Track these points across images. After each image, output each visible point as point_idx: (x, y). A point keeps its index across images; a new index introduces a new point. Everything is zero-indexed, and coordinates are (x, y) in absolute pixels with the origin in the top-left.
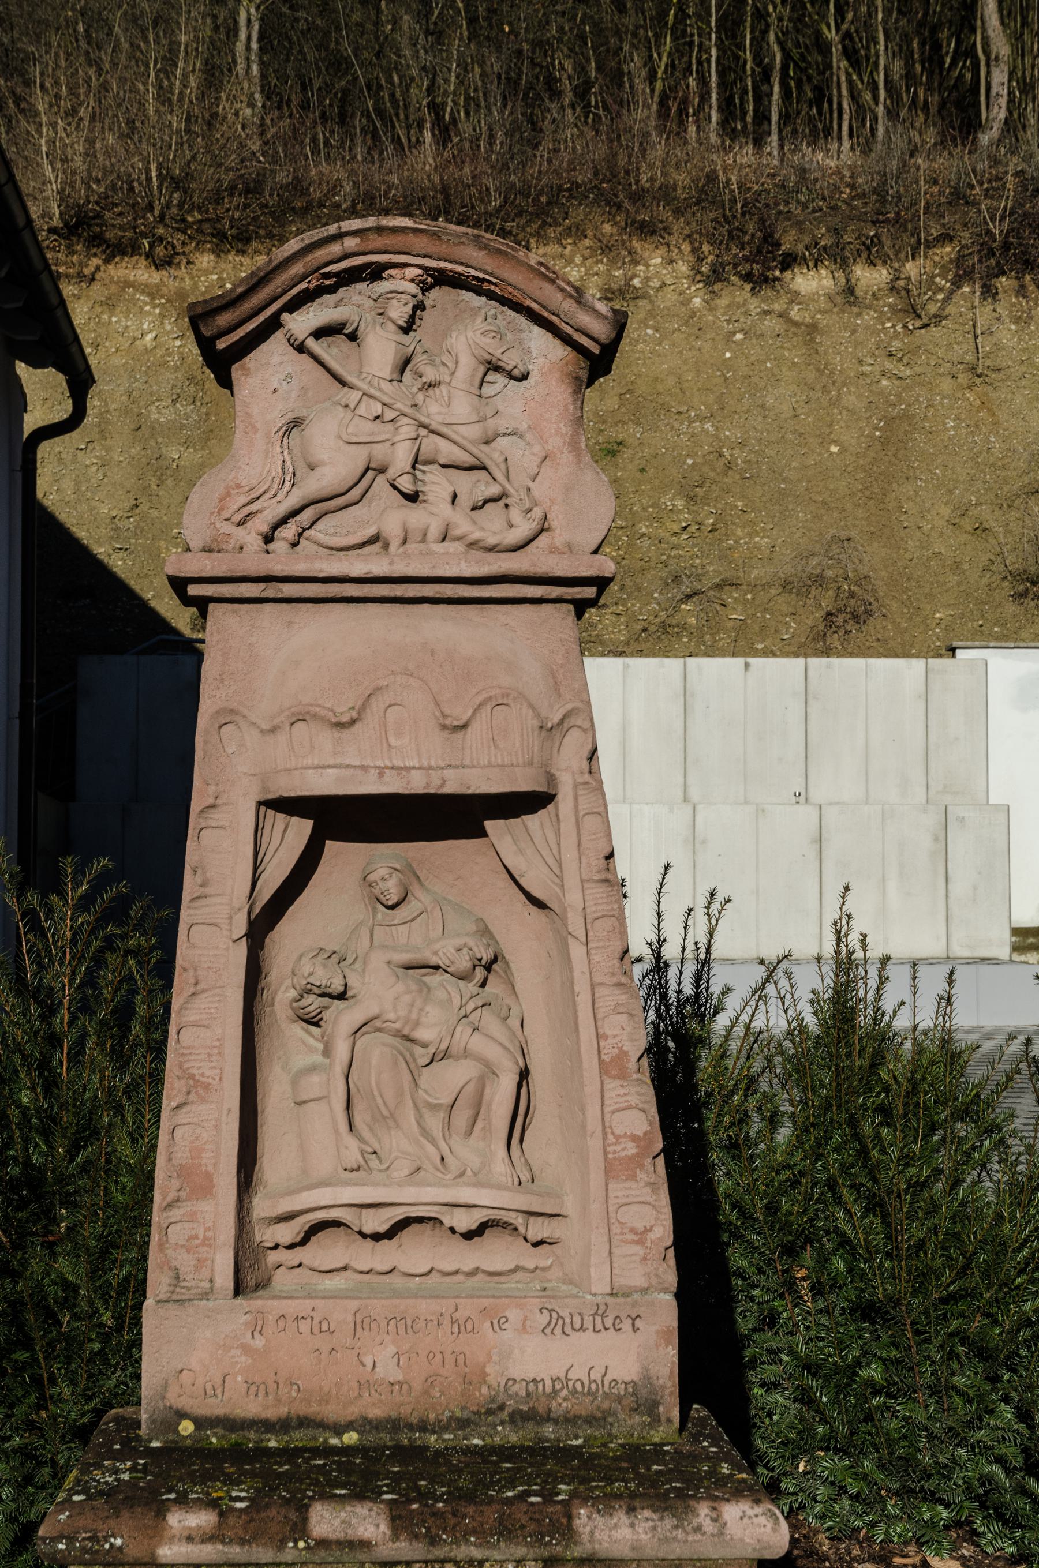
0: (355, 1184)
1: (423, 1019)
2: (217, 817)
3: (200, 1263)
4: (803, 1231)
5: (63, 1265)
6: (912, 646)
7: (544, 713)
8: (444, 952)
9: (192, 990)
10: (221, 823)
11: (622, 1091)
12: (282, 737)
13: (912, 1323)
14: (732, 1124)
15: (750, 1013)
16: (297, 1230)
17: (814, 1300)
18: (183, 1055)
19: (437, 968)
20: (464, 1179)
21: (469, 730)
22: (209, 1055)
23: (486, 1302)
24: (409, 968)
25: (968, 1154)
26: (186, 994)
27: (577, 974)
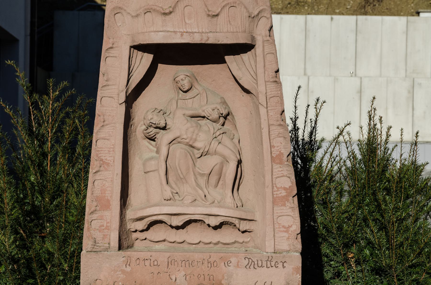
0: (169, 206)
1: (198, 138)
2: (113, 52)
3: (105, 236)
4: (352, 239)
5: (48, 245)
6: (401, 11)
7: (251, 11)
8: (207, 110)
9: (102, 124)
10: (115, 55)
11: (280, 169)
12: (141, 19)
13: (397, 276)
14: (324, 194)
15: (333, 148)
16: (145, 224)
17: (356, 267)
18: (98, 151)
19: (204, 117)
20: (214, 204)
21: (219, 17)
22: (109, 151)
23: (222, 255)
24: (192, 117)
25: (422, 208)
26: (100, 125)
27: (262, 120)
